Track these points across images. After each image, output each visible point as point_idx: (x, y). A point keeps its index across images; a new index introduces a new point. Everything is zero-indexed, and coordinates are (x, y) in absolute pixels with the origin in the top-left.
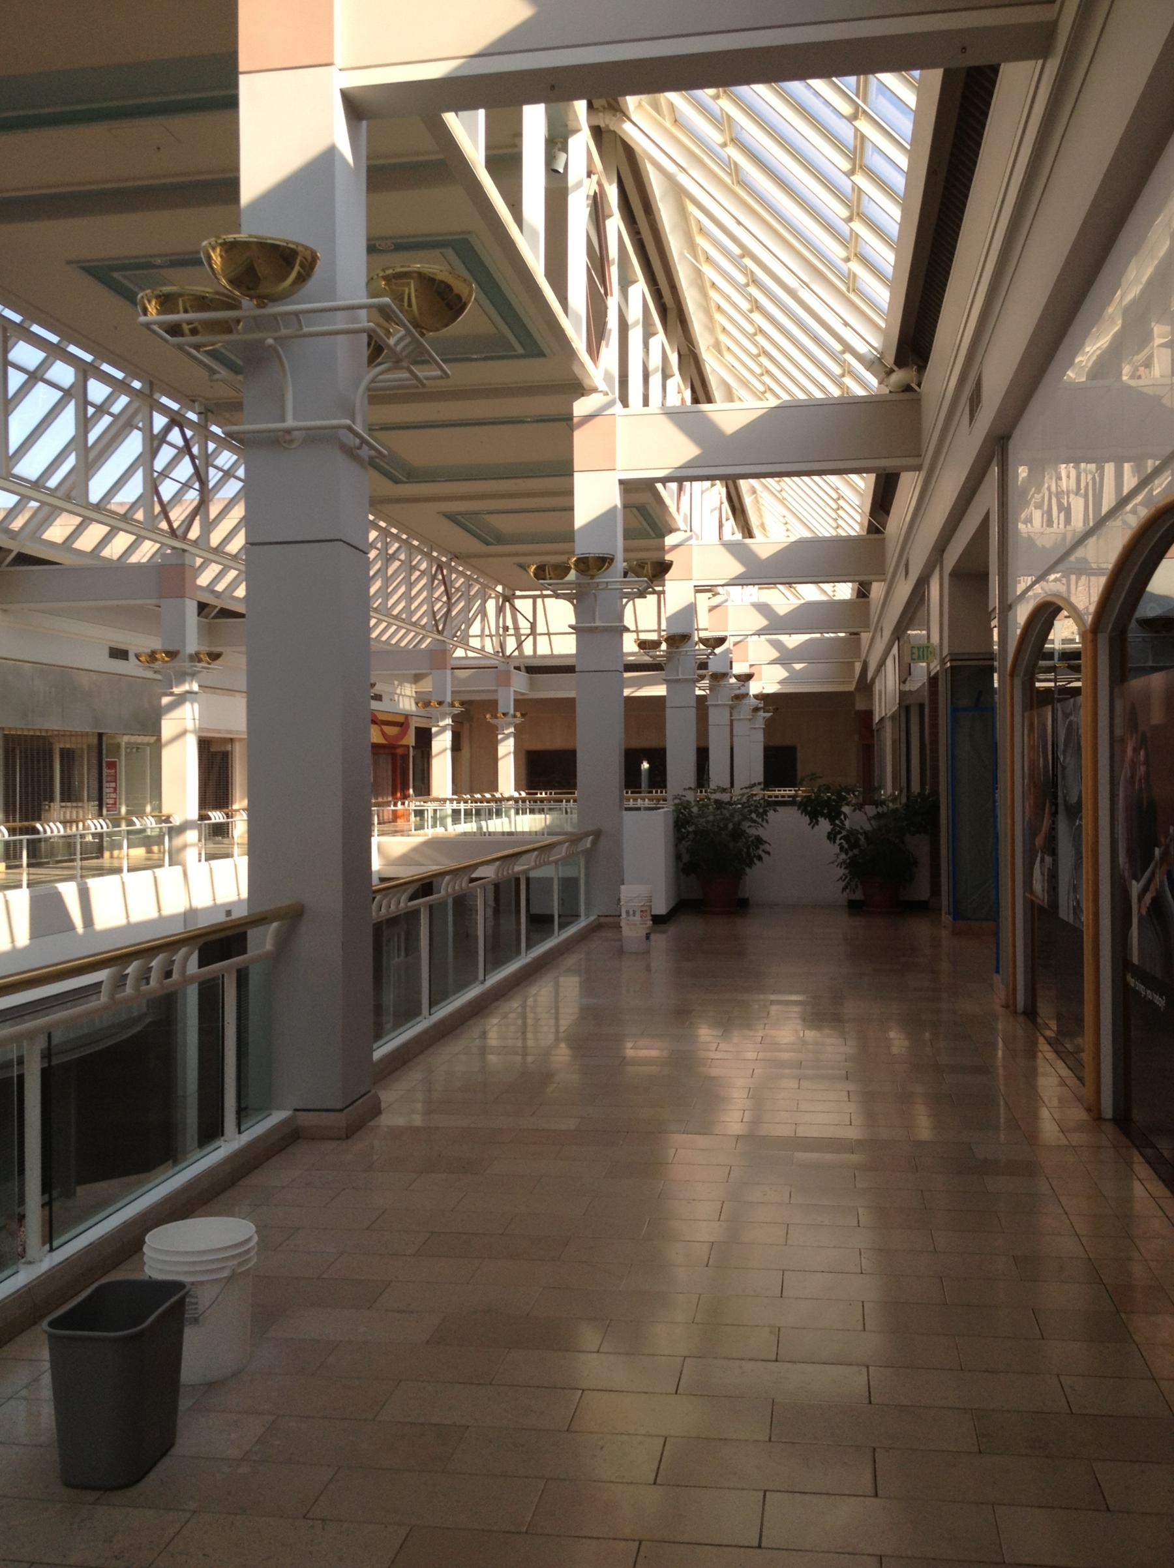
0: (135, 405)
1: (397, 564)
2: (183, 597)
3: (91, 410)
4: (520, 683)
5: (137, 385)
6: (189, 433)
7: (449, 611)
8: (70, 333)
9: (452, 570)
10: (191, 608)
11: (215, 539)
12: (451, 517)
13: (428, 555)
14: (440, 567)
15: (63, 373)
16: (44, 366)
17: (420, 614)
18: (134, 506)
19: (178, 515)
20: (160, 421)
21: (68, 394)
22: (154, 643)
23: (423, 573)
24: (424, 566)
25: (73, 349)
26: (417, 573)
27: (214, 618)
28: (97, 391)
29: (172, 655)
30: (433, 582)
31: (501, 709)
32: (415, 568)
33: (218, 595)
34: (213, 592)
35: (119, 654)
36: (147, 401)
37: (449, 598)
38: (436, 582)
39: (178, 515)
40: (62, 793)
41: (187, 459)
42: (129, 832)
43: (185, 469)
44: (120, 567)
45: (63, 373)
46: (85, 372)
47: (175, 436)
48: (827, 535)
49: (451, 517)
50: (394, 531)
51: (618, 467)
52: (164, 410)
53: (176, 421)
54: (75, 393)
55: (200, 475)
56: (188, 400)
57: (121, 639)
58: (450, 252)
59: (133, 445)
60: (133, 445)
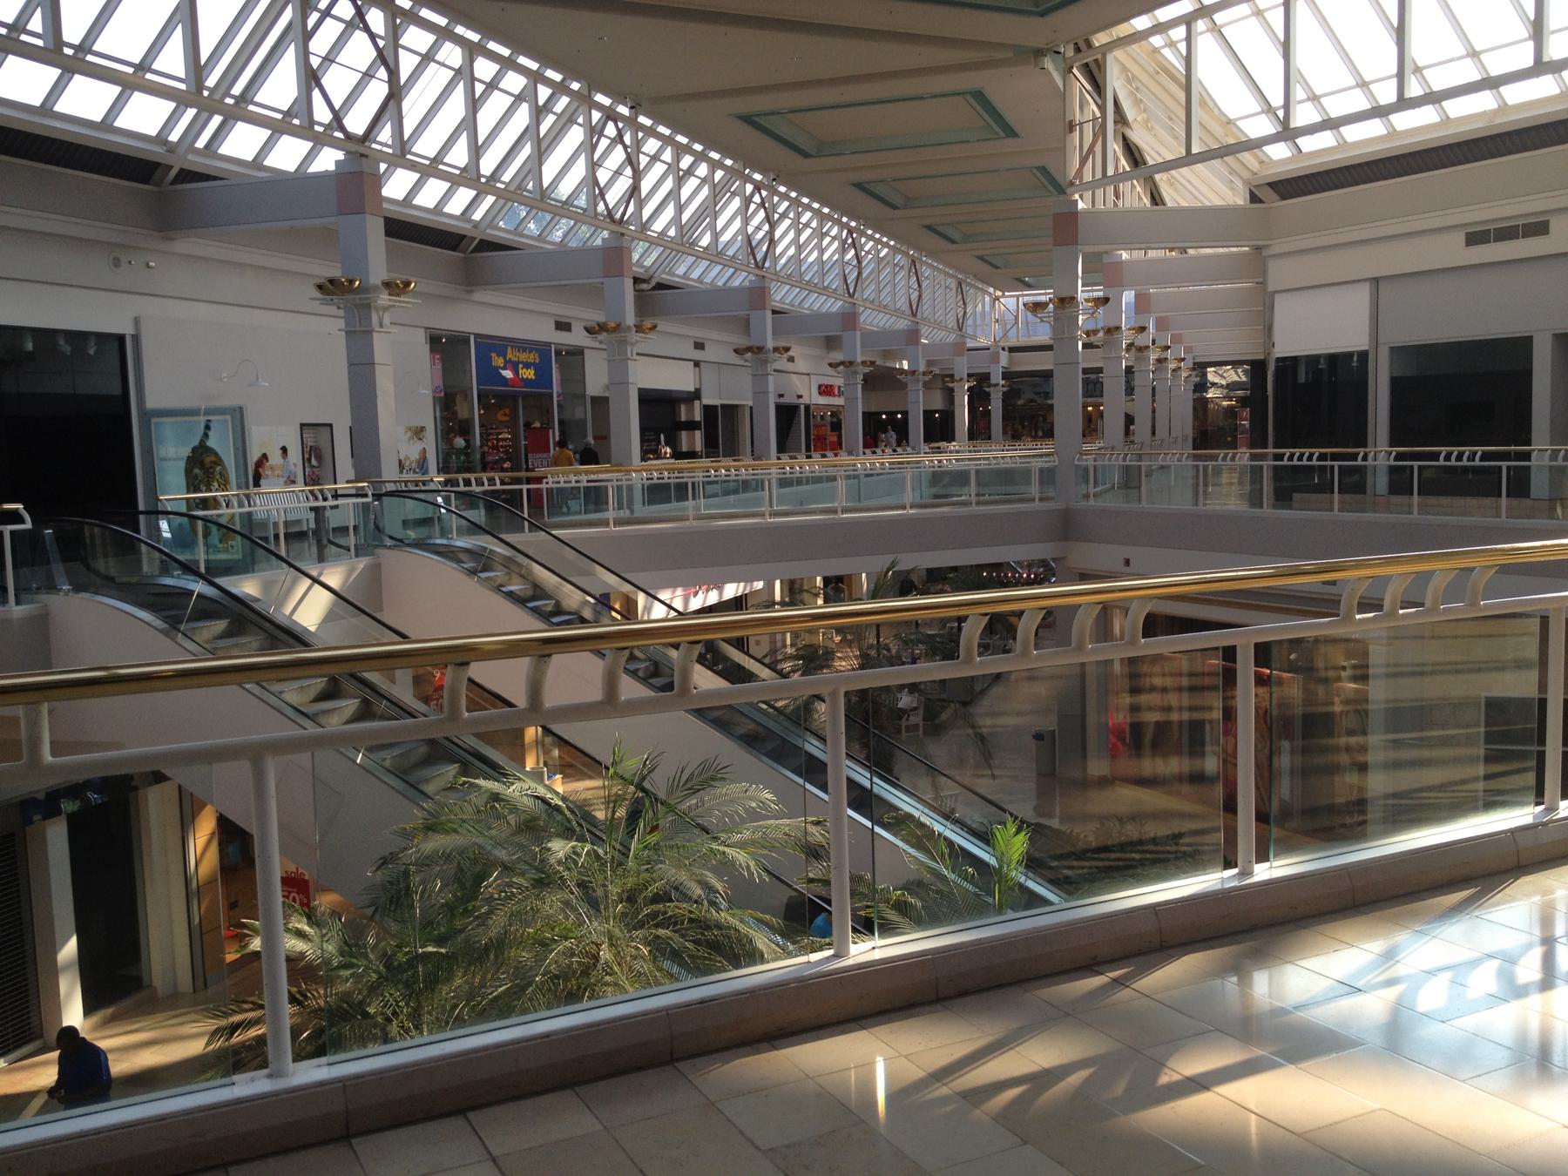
0: (575, 104)
1: (808, 232)
2: (361, 211)
3: (479, 88)
4: (1004, 358)
5: (575, 86)
6: (620, 125)
7: (860, 274)
8: (520, 47)
9: (863, 234)
10: (375, 228)
11: (487, 166)
12: (747, 119)
13: (838, 222)
14: (850, 232)
15: (452, 54)
16: (435, 48)
17: (902, 303)
18: (575, 193)
19: (613, 197)
20: (596, 116)
21: (519, 98)
22: (599, 317)
23: (834, 238)
24: (834, 232)
25: (460, 30)
26: (828, 239)
27: (174, 182)
28: (485, 69)
29: (851, 363)
30: (305, 18)
31: (993, 381)
32: (827, 234)
33: (172, 148)
34: (166, 143)
35: (563, 326)
36: (584, 101)
37: (859, 262)
38: (753, 206)
39: (613, 197)
40: (1276, 436)
41: (620, 147)
42: (783, 483)
43: (618, 155)
44: (300, 181)
45: (452, 54)
46: (536, 78)
47: (611, 130)
48: (1218, 202)
49: (747, 119)
50: (805, 200)
51: (1532, 692)
52: (600, 107)
53: (610, 115)
54: (464, 74)
55: (631, 161)
56: (619, 97)
57: (566, 311)
58: (969, 97)
59: (576, 135)
60: (576, 135)
